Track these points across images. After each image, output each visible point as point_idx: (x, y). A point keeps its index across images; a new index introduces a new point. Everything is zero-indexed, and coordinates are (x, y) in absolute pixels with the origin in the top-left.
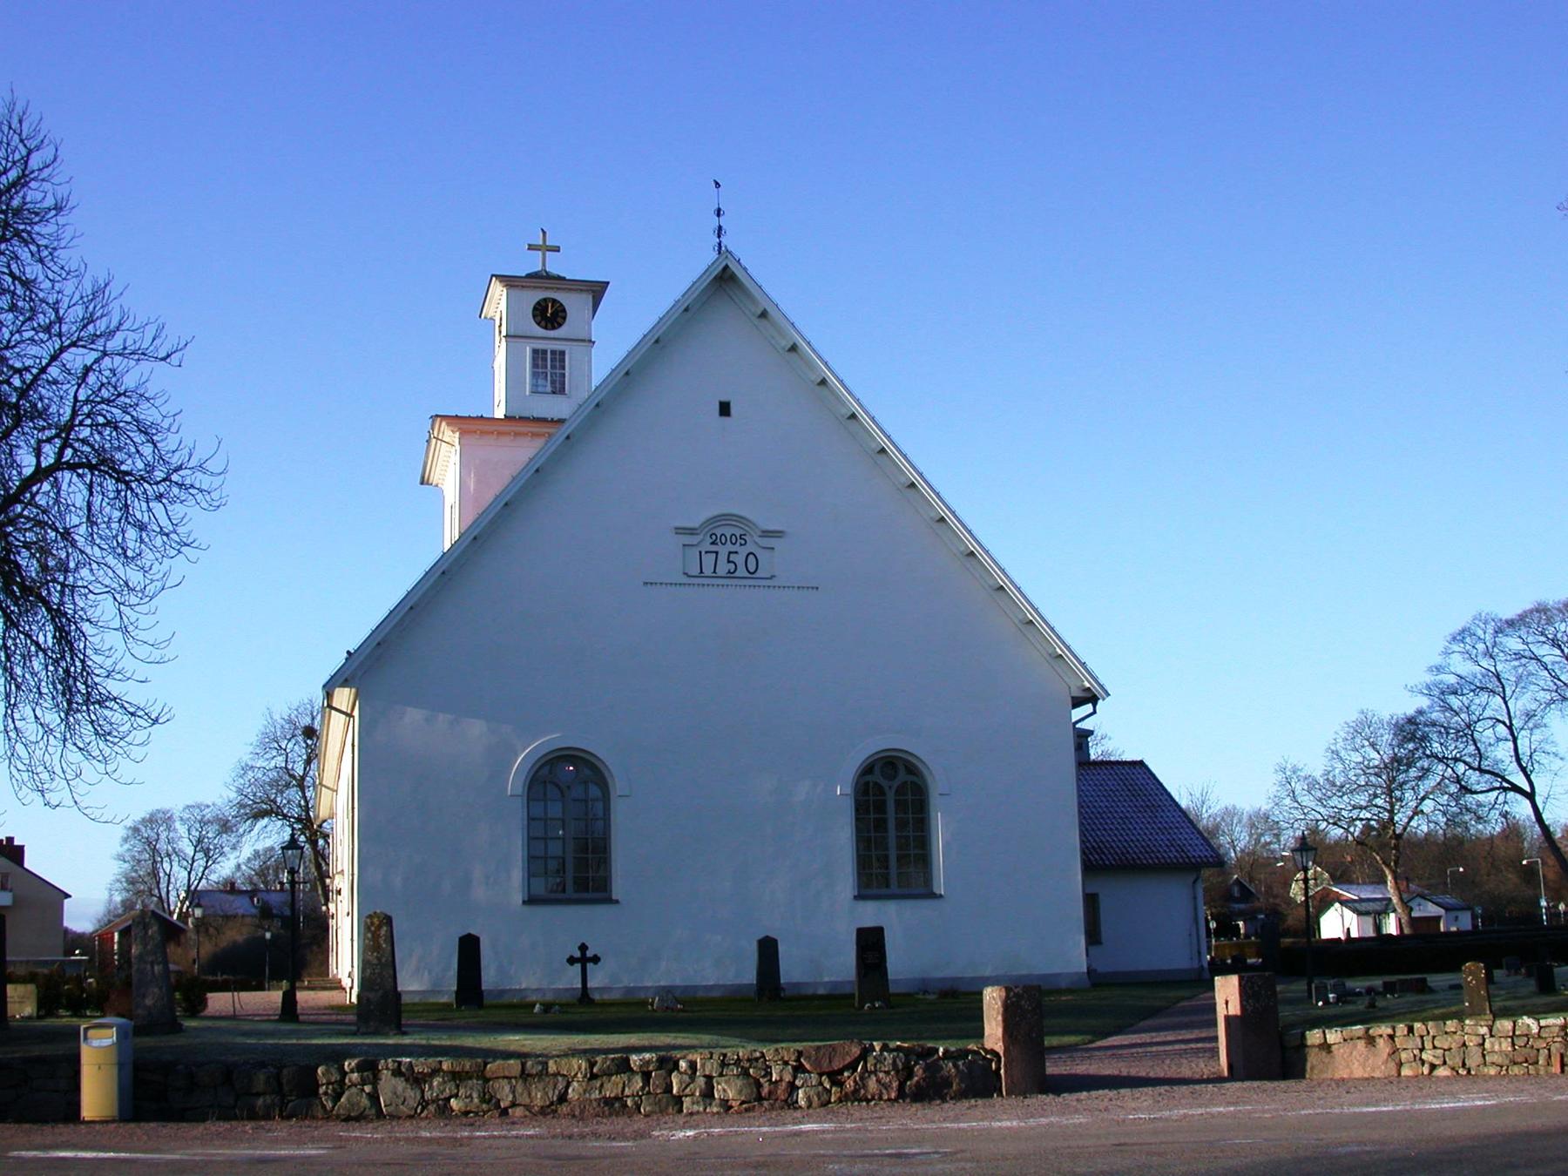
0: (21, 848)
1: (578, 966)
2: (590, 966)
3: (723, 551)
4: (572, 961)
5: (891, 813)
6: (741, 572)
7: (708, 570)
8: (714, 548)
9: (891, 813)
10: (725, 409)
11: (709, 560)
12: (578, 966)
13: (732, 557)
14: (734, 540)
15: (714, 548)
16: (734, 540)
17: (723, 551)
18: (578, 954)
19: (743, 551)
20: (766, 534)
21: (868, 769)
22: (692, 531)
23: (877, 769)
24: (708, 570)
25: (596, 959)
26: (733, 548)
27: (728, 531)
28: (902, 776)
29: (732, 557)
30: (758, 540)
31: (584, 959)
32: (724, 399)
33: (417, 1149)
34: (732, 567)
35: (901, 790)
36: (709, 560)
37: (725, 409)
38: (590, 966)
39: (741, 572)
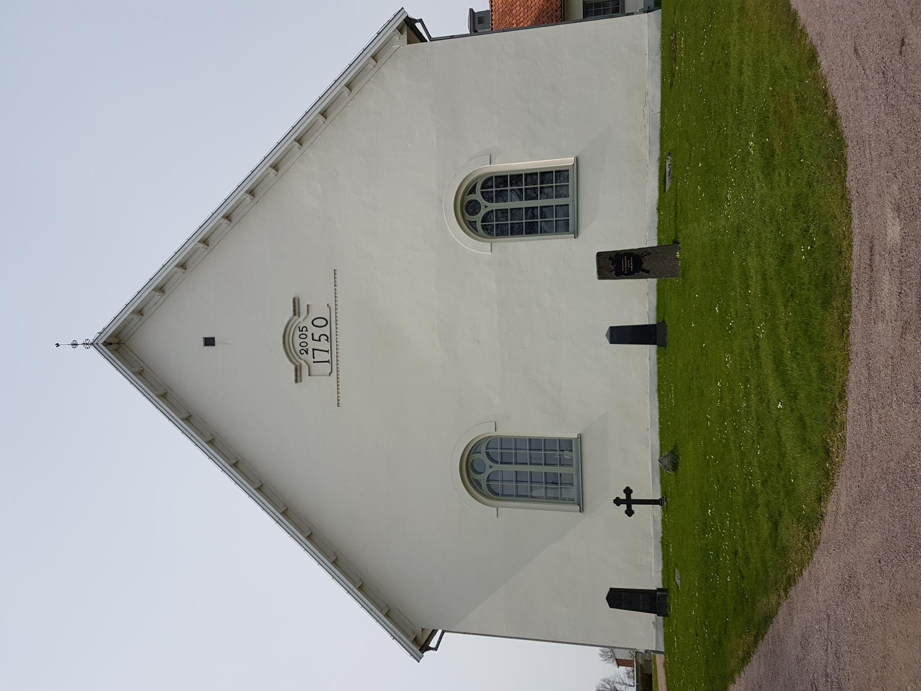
0: (618, 666)
1: (634, 507)
2: (633, 497)
3: (312, 345)
4: (630, 512)
5: (514, 204)
6: (326, 330)
7: (326, 357)
8: (310, 352)
9: (514, 204)
10: (209, 342)
11: (320, 356)
12: (634, 507)
13: (316, 337)
14: (303, 336)
15: (310, 352)
16: (303, 336)
17: (312, 345)
18: (624, 507)
19: (312, 329)
20: (296, 312)
21: (471, 227)
22: (298, 371)
23: (472, 218)
24: (326, 357)
25: (628, 491)
26: (310, 337)
27: (298, 341)
28: (477, 196)
29: (316, 337)
30: (302, 317)
31: (628, 501)
32: (202, 342)
33: (734, 64)
34: (323, 338)
35: (488, 197)
36: (320, 356)
37: (209, 342)
38: (633, 497)
39: (326, 330)
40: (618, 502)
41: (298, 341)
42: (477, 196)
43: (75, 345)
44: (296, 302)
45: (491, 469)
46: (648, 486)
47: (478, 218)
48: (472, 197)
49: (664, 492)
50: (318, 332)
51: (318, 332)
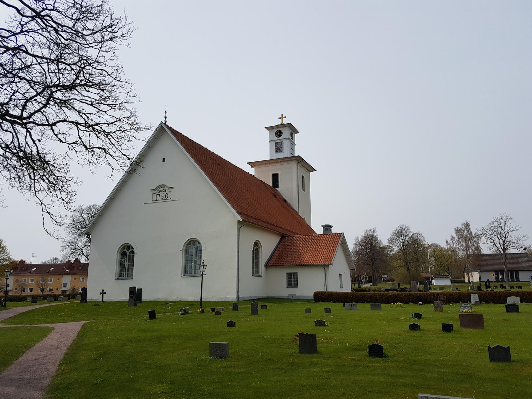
3: (161, 194)
6: (164, 198)
10: (164, 160)
19: (165, 193)
20: (169, 188)
21: (199, 243)
27: (162, 189)
28: (131, 250)
31: (103, 293)
37: (164, 160)
39: (164, 198)
40: (103, 290)
41: (162, 189)
42: (131, 250)
43: (166, 112)
44: (172, 188)
45: (128, 252)
46: (106, 298)
47: (126, 250)
48: (124, 250)
49: (106, 302)
50: (164, 195)
51: (164, 195)
